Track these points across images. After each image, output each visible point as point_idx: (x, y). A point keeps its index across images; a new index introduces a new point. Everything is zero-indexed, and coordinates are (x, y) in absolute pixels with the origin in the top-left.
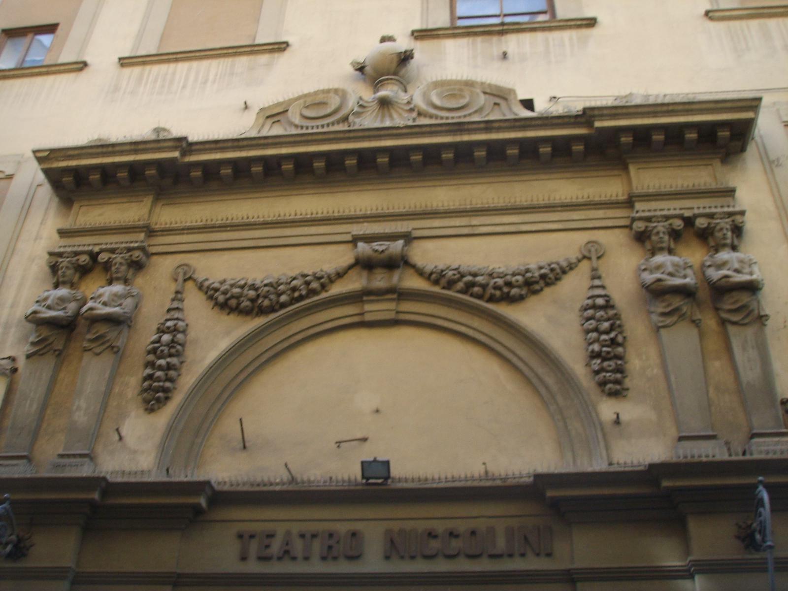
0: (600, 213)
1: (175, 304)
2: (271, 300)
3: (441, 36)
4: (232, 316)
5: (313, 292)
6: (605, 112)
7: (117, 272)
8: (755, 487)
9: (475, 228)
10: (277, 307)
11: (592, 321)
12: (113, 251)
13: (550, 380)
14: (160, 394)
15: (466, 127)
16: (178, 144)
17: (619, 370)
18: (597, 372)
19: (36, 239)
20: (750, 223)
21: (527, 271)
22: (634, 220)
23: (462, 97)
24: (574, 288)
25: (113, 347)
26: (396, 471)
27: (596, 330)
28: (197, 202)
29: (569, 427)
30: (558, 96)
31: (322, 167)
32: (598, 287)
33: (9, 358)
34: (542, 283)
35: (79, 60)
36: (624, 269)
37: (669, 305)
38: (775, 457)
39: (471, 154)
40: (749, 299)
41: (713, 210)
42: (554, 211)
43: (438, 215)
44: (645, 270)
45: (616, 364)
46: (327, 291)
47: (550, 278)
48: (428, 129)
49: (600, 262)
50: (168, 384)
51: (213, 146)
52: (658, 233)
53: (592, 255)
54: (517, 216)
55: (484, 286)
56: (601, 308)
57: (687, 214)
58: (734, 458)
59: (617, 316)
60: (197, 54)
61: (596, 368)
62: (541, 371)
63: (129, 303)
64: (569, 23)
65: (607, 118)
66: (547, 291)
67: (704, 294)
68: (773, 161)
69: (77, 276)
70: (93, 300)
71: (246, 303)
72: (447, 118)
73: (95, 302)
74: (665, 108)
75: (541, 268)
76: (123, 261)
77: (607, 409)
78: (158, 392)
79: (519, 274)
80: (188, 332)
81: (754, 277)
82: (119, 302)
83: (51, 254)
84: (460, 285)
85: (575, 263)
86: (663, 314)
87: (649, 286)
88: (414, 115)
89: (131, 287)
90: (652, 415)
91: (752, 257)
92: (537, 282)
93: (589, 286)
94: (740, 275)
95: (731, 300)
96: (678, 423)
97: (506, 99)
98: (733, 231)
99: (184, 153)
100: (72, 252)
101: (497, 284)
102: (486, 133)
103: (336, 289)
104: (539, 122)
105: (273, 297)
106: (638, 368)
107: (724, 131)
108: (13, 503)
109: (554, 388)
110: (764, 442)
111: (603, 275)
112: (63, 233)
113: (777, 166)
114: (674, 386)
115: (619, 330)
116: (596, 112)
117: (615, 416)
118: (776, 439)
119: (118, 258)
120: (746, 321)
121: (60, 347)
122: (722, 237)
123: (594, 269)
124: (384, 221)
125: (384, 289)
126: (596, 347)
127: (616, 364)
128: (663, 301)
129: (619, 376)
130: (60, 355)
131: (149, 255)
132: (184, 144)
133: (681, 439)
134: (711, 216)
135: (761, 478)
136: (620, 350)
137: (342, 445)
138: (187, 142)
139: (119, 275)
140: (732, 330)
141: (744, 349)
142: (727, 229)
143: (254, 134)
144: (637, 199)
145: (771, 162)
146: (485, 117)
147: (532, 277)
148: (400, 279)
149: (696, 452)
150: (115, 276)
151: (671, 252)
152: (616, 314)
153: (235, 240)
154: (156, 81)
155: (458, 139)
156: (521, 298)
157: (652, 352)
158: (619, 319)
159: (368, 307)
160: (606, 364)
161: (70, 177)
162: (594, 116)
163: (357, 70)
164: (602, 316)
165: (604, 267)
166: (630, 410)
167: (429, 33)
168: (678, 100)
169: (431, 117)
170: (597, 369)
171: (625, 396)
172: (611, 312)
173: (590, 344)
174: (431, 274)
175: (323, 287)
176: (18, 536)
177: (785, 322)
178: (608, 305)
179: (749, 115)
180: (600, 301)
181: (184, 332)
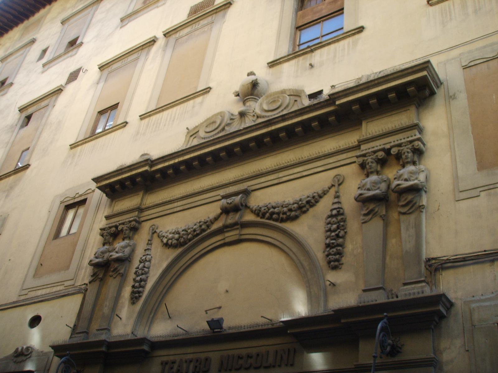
1: (336, 200)
2: (184, 238)
3: (282, 62)
4: (170, 249)
5: (204, 230)
6: (340, 94)
7: (370, 168)
9: (280, 179)
10: (188, 241)
12: (123, 224)
13: (306, 264)
14: (137, 295)
15: (272, 121)
16: (146, 162)
17: (340, 253)
19: (100, 222)
21: (301, 200)
23: (278, 101)
24: (325, 206)
25: (120, 273)
26: (225, 325)
29: (311, 290)
30: (334, 84)
31: (394, 96)
32: (336, 203)
33: (84, 284)
34: (308, 206)
35: (207, 87)
37: (368, 209)
38: (412, 297)
41: (400, 142)
42: (321, 160)
43: (150, 209)
45: (337, 250)
46: (210, 229)
47: (312, 203)
48: (255, 127)
49: (341, 187)
50: (141, 289)
51: (162, 160)
52: (368, 163)
53: (339, 182)
55: (278, 214)
56: (336, 216)
57: (388, 146)
58: (391, 300)
59: (344, 220)
60: (171, 105)
62: (302, 258)
63: (127, 250)
64: (348, 34)
65: (343, 97)
66: (311, 210)
68: (451, 97)
69: (111, 239)
70: (396, 180)
71: (175, 242)
72: (271, 116)
73: (362, 190)
74: (373, 83)
76: (127, 228)
77: (332, 276)
78: (136, 294)
79: (296, 203)
80: (151, 261)
82: (415, 177)
83: (101, 229)
84: (268, 215)
85: (327, 190)
87: (393, 189)
88: (255, 117)
89: (382, 175)
92: (305, 206)
95: (403, 199)
97: (300, 96)
99: (151, 166)
100: (128, 221)
101: (284, 211)
102: (283, 122)
103: (215, 227)
104: (308, 109)
105: (184, 237)
107: (411, 87)
108: (389, 319)
111: (341, 195)
112: (107, 218)
113: (453, 99)
115: (342, 228)
116: (336, 96)
118: (413, 286)
119: (405, 149)
120: (411, 211)
121: (384, 213)
124: (272, 174)
125: (237, 223)
126: (328, 241)
127: (337, 250)
129: (337, 257)
130: (101, 280)
131: (140, 223)
132: (149, 162)
134: (400, 145)
135: (385, 314)
136: (341, 240)
137: (208, 312)
138: (151, 160)
139: (372, 170)
140: (403, 217)
141: (407, 229)
142: (408, 152)
143: (184, 148)
144: (362, 143)
146: (290, 110)
147: (302, 203)
148: (241, 217)
150: (370, 171)
151: (378, 173)
152: (342, 219)
153: (153, 214)
154: (154, 125)
155: (270, 129)
156: (296, 218)
159: (227, 235)
161: (357, 105)
163: (237, 96)
164: (334, 222)
167: (276, 62)
168: (389, 72)
169: (263, 117)
171: (340, 269)
172: (339, 218)
174: (255, 210)
175: (208, 227)
176: (77, 370)
177: (439, 206)
179: (425, 73)
180: (334, 212)
181: (150, 261)
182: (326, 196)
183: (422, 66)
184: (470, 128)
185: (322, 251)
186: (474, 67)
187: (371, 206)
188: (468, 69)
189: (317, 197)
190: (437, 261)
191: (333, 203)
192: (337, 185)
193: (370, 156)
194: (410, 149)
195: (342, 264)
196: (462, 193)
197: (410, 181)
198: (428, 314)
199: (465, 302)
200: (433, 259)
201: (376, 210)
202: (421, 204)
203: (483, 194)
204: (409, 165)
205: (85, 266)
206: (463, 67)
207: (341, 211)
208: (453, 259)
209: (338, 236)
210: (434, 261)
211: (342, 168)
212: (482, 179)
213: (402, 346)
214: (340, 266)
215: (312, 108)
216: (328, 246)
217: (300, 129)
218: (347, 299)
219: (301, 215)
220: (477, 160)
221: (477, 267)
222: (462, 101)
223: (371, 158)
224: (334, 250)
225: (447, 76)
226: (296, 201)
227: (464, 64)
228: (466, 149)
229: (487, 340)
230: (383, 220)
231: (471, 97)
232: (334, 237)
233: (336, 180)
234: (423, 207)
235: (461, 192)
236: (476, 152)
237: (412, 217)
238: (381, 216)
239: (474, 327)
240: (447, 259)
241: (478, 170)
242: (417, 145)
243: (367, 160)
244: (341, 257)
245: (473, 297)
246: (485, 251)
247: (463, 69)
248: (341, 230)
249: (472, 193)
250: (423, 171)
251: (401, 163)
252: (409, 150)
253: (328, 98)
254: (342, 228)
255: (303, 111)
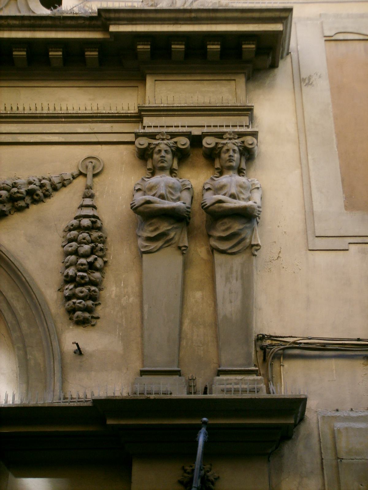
0: (106, 127)
6: (122, 15)
8: (197, 428)
11: (74, 244)
13: (18, 305)
17: (93, 297)
18: (68, 298)
20: (265, 146)
21: (14, 185)
22: (137, 135)
24: (63, 207)
27: (75, 252)
28: (158, 74)
29: (29, 357)
32: (87, 206)
34: (28, 200)
36: (120, 187)
37: (156, 230)
39: (204, 48)
40: (241, 227)
44: (139, 190)
45: (89, 290)
47: (37, 195)
49: (96, 179)
52: (160, 151)
53: (92, 171)
54: (15, 125)
56: (87, 229)
57: (196, 132)
58: (193, 396)
61: (67, 293)
67: (199, 219)
68: (304, 80)
74: (187, 15)
75: (30, 183)
77: (71, 337)
81: (250, 203)
86: (149, 239)
90: (118, 346)
91: (256, 182)
92: (23, 199)
93: (79, 205)
94: (234, 201)
96: (143, 357)
98: (241, 154)
104: (49, 22)
106: (113, 296)
109: (21, 313)
110: (228, 380)
111: (97, 194)
113: (307, 85)
114: (146, 317)
115: (101, 254)
116: (112, 15)
117: (75, 347)
118: (239, 377)
122: (228, 158)
123: (89, 188)
126: (71, 271)
127: (89, 290)
128: (151, 225)
129: (90, 303)
133: (143, 373)
134: (220, 135)
135: (205, 419)
136: (97, 275)
139: (165, 165)
140: (218, 258)
141: (227, 279)
142: (234, 151)
145: (302, 80)
147: (18, 192)
149: (154, 388)
151: (172, 172)
152: (100, 237)
157: (132, 279)
158: (104, 242)
160: (79, 289)
162: (109, 19)
164: (84, 239)
165: (99, 185)
166: (91, 340)
170: (67, 294)
171: (93, 325)
172: (95, 234)
173: (67, 267)
178: (95, 226)
179: (278, 27)
180: (86, 222)
182: (65, 190)
183: (277, 14)
184: (334, 137)
185: (57, 287)
186: (343, 43)
187: (164, 227)
188: (333, 43)
189: (48, 187)
190: (274, 342)
191: (82, 206)
192: (90, 175)
193: (163, 139)
194: (238, 146)
195: (98, 318)
196: (317, 240)
197: (239, 199)
198: (266, 429)
199: (323, 417)
200: (270, 337)
201: (172, 235)
202: (253, 243)
203: (353, 248)
204: (231, 173)
205: (180, 203)
206: (325, 37)
207: (99, 224)
208: (305, 343)
209: (91, 266)
210: (268, 342)
211: (99, 146)
212: (353, 224)
213: (216, 479)
214: (94, 322)
215: (58, 22)
216: (69, 280)
217: (25, 53)
218: (110, 382)
219: (12, 213)
220: (344, 192)
221: (341, 363)
222: (321, 93)
223: (166, 144)
224: (85, 289)
225: (297, 45)
226: (5, 185)
227: (327, 34)
228: (327, 172)
229: (361, 485)
230: (183, 254)
231: (337, 89)
232: (84, 267)
233: (90, 166)
234: (258, 248)
235: (316, 237)
236: (343, 181)
237: (237, 261)
238: (180, 248)
239: (341, 461)
240: (294, 343)
241: (346, 208)
242: (250, 143)
243: (157, 145)
244: (96, 305)
245: (337, 410)
246: (359, 340)
247: (326, 40)
248: (99, 256)
249: (337, 243)
250: (258, 188)
251: (150, 165)
252: (236, 148)
253: (96, 15)
254: (101, 254)
255: (38, 22)
